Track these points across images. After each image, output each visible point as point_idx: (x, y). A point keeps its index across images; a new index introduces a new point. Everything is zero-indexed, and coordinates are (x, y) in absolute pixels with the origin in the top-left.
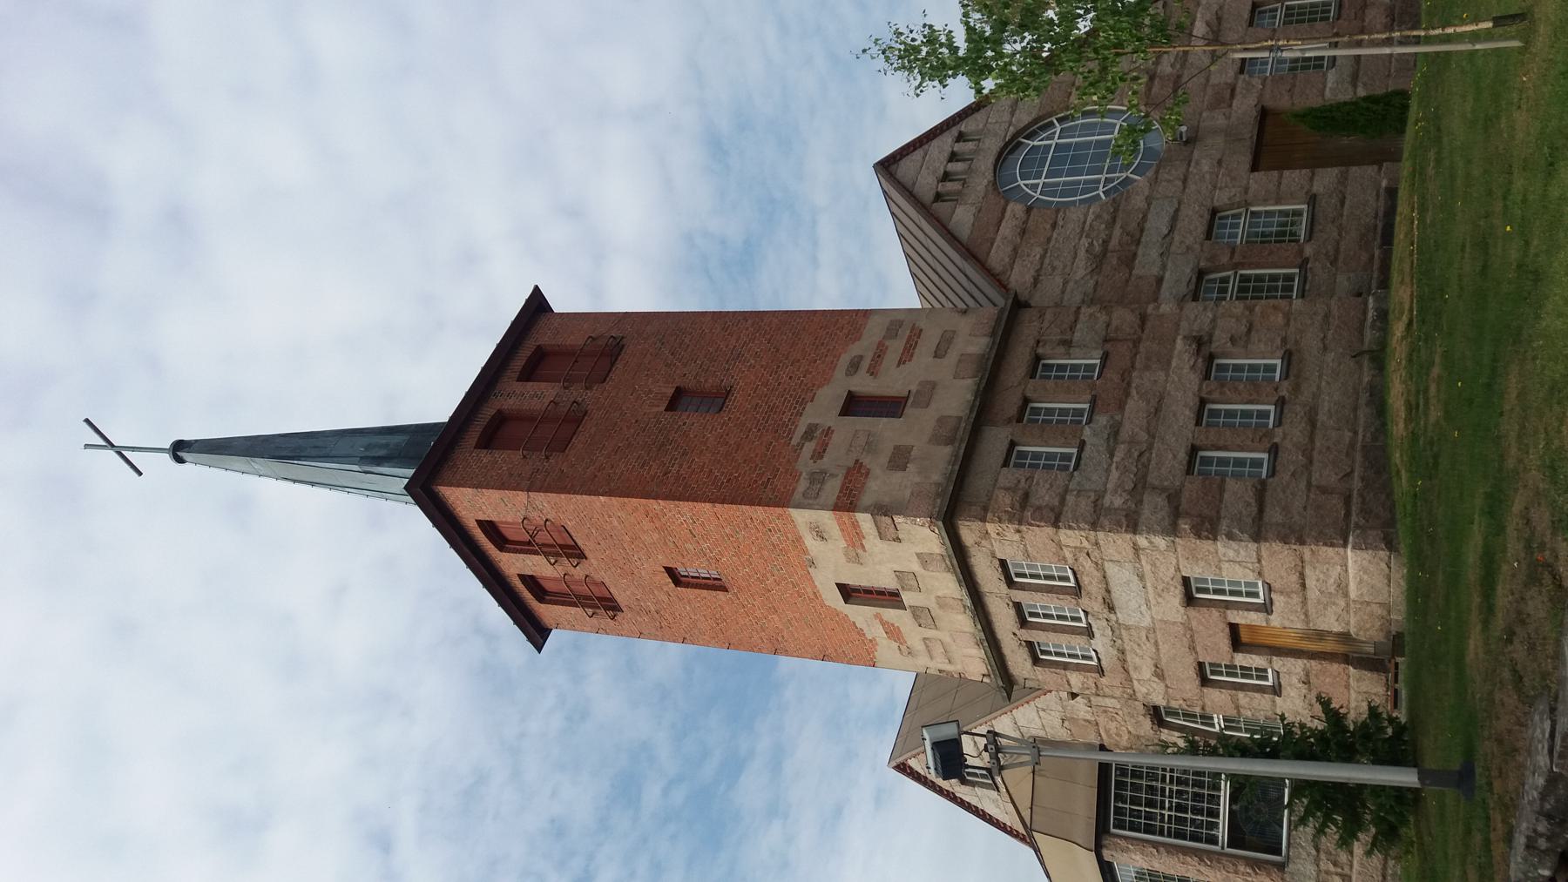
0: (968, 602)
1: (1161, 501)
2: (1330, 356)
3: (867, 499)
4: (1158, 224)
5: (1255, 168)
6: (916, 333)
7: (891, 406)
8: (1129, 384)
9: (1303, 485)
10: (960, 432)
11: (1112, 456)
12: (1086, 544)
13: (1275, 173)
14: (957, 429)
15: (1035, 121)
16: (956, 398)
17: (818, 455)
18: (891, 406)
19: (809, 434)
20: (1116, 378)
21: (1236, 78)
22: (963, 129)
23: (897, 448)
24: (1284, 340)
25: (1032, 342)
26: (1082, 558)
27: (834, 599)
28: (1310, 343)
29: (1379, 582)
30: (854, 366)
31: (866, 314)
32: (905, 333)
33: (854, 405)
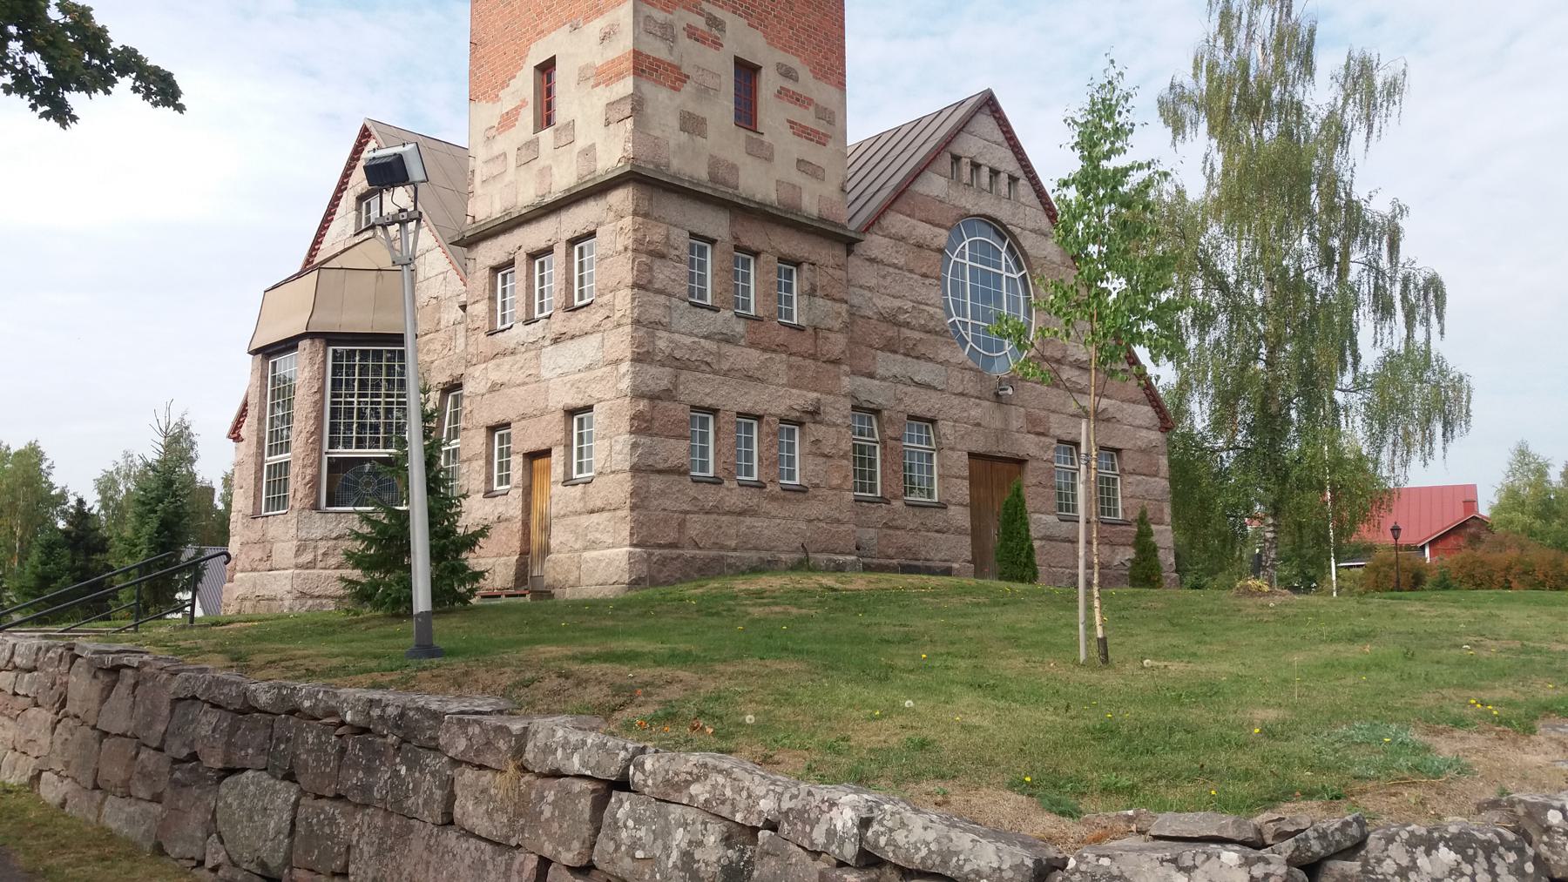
0: (548, 200)
1: (665, 383)
3: (648, 88)
5: (971, 455)
6: (820, 139)
7: (746, 114)
8: (774, 351)
9: (685, 507)
10: (723, 189)
11: (706, 337)
12: (618, 314)
13: (967, 473)
14: (725, 184)
15: (1024, 254)
17: (692, 33)
18: (746, 114)
19: (713, 22)
20: (779, 340)
22: (1021, 181)
23: (704, 120)
24: (817, 486)
25: (813, 258)
26: (604, 312)
27: (538, 55)
28: (815, 509)
29: (599, 576)
30: (788, 73)
31: (842, 85)
33: (746, 72)
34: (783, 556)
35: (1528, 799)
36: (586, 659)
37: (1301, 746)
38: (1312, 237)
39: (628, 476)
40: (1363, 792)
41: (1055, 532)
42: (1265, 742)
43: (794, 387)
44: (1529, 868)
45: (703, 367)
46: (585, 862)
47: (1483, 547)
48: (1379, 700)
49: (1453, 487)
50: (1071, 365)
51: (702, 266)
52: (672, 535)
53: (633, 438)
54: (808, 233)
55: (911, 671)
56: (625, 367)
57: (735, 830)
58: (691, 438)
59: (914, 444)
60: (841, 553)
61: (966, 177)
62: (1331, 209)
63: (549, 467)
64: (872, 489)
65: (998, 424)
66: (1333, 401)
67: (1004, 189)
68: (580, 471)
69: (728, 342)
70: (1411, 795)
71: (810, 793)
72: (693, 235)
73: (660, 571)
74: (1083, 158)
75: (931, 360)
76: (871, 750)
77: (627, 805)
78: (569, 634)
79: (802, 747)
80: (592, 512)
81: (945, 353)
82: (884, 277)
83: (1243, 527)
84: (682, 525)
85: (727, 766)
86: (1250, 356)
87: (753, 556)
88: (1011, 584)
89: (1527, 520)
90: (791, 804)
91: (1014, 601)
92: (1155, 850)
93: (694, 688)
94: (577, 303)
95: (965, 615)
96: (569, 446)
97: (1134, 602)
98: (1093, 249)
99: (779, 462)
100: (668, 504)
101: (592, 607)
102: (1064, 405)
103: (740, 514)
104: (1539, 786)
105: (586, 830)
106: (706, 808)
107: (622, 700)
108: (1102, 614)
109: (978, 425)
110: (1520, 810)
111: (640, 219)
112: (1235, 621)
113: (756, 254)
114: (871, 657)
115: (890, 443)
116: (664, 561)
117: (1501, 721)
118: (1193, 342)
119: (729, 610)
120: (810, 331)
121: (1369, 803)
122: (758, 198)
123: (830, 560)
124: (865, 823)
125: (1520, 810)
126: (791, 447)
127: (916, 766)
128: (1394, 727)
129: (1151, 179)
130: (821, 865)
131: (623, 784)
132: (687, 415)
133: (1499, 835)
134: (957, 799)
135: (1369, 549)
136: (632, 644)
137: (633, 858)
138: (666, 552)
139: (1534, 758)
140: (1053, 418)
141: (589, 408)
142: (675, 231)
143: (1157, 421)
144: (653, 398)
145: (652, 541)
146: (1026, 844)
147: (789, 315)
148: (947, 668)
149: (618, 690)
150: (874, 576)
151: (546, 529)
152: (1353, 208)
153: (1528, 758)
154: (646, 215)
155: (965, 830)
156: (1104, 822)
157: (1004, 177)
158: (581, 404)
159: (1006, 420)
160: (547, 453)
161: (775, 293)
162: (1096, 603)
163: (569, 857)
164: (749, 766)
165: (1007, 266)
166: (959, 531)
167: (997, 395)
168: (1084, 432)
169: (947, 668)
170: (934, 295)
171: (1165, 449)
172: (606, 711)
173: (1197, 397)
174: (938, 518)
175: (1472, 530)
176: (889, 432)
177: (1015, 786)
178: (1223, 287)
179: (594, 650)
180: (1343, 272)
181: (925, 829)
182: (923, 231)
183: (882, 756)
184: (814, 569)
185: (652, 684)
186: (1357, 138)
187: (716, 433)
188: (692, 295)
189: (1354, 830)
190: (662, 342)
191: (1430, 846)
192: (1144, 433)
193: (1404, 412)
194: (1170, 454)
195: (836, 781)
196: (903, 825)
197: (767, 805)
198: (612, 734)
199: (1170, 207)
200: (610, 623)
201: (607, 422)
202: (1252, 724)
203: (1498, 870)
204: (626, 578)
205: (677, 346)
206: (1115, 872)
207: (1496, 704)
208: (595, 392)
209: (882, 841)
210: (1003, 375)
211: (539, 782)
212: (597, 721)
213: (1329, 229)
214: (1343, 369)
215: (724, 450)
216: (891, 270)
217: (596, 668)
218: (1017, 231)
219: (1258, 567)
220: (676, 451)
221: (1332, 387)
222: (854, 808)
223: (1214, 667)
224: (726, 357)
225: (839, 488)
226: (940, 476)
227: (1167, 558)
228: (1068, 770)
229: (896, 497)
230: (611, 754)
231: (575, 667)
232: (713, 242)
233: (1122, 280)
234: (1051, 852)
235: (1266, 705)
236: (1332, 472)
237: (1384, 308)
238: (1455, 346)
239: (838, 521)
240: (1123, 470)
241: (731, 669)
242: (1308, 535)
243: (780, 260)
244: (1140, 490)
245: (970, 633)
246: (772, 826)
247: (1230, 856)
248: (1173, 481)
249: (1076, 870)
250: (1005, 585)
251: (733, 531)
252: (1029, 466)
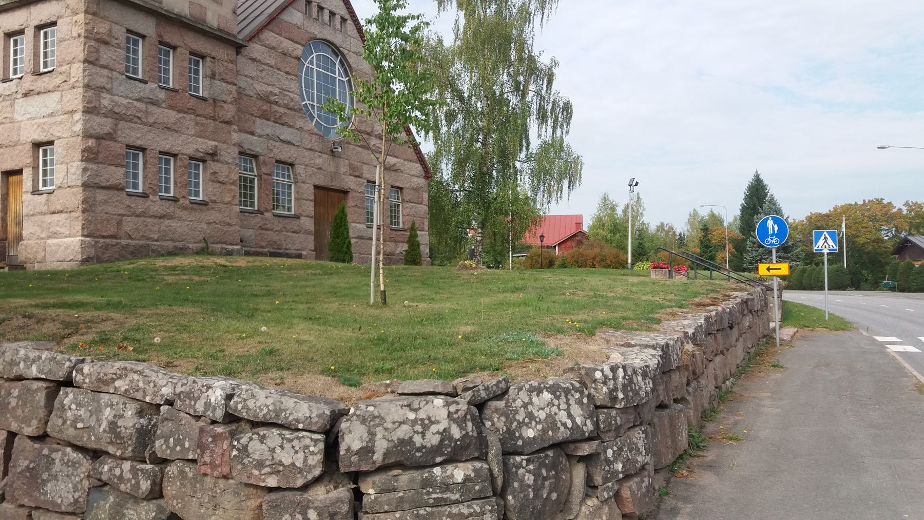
1: (107, 129)
4: (286, 133)
5: (316, 187)
8: (186, 112)
9: (122, 212)
11: (137, 100)
12: (73, 80)
13: (312, 198)
20: (189, 105)
24: (214, 202)
25: (213, 54)
28: (213, 216)
29: (60, 256)
34: (190, 246)
35: (587, 366)
36: (46, 306)
37: (481, 344)
38: (509, 74)
39: (80, 190)
40: (510, 366)
42: (464, 343)
43: (200, 137)
44: (585, 400)
45: (135, 120)
46: (41, 432)
47: (583, 247)
48: (524, 321)
49: (572, 216)
51: (135, 52)
52: (112, 230)
53: (84, 165)
55: (269, 312)
56: (78, 116)
57: (145, 406)
58: (127, 166)
59: (280, 178)
60: (231, 244)
61: (315, 14)
62: (521, 59)
63: (21, 182)
64: (252, 205)
65: (332, 169)
66: (515, 167)
67: (338, 25)
68: (45, 184)
70: (532, 367)
71: (194, 382)
72: (129, 31)
73: (103, 254)
74: (380, 8)
75: (291, 126)
76: (238, 357)
77: (71, 396)
78: (35, 292)
79: (193, 356)
80: (54, 213)
81: (300, 123)
82: (261, 71)
83: (466, 234)
84: (119, 223)
85: (140, 368)
86: (473, 140)
87: (170, 245)
88: (337, 264)
89: (605, 233)
90: (182, 389)
91: (337, 272)
92: (399, 400)
93: (122, 324)
94: (42, 70)
95: (307, 280)
96: (36, 168)
97: (405, 273)
98: (385, 64)
99: (189, 185)
100: (110, 209)
101: (54, 276)
103: (161, 218)
104: (594, 360)
105: (42, 413)
106: (126, 394)
107: (70, 331)
108: (384, 276)
109: (320, 169)
110: (583, 372)
111: (90, 17)
112: (457, 282)
113: (174, 48)
114: (244, 304)
115: (264, 177)
116: (106, 247)
117: (581, 330)
118: (444, 129)
119: (151, 278)
120: (211, 101)
121: (512, 372)
122: (176, 11)
123: (223, 248)
124: (229, 397)
125: (583, 372)
126: (197, 176)
127: (268, 364)
128: (529, 333)
129: (419, 26)
130: (201, 424)
131: (68, 382)
132: (124, 151)
133: (572, 385)
134: (289, 381)
135: (529, 247)
136: (79, 298)
137: (76, 428)
138: (108, 240)
139: (593, 347)
140: (365, 167)
141: (51, 143)
142: (116, 28)
143: (423, 173)
144: (99, 138)
145: (98, 233)
146: (327, 403)
147: (197, 89)
148: (292, 309)
149: (66, 325)
150: (251, 259)
151: (19, 224)
152: (531, 58)
153: (590, 347)
154: (94, 14)
155: (291, 397)
156: (373, 388)
157: (338, 18)
158: (45, 139)
159: (337, 167)
160: (19, 172)
161: (187, 74)
162: (381, 271)
163: (29, 430)
164: (155, 368)
165: (339, 73)
166: (307, 232)
167: (332, 151)
168: (378, 175)
169: (292, 309)
170: (294, 86)
171: (426, 189)
172: (58, 339)
173: (445, 161)
174: (294, 225)
175: (579, 238)
176: (264, 170)
177: (326, 372)
178: (461, 99)
179: (52, 301)
180: (524, 96)
181: (267, 398)
182: (287, 44)
183: (244, 360)
184: (212, 254)
185: (91, 321)
186: (537, 19)
187: (144, 164)
188: (128, 71)
189: (503, 385)
190: (106, 101)
191: (539, 391)
192: (416, 179)
193: (550, 174)
194: (429, 191)
195: (213, 374)
196: (253, 396)
197: (166, 391)
198: (62, 352)
199: (435, 49)
200: (65, 285)
201: (65, 152)
202: (458, 334)
203: (570, 402)
204: (79, 257)
205: (117, 104)
206: (376, 414)
207: (579, 322)
208: (55, 132)
209: (240, 406)
210: (336, 139)
211: (7, 384)
212: (50, 345)
213: (518, 70)
214: (521, 150)
215: (150, 175)
216: (266, 67)
217: (52, 312)
218: (346, 52)
219: (472, 255)
220: (116, 175)
221: (515, 159)
222: (222, 389)
223: (442, 305)
224: (152, 114)
225: (229, 203)
226: (296, 199)
227: (425, 250)
228: (356, 362)
229: (267, 211)
230: (60, 364)
231: (36, 311)
232: (143, 37)
233: (402, 84)
234: (342, 406)
235: (467, 324)
236: (512, 205)
237: (542, 118)
238: (576, 139)
239: (229, 224)
240: (403, 200)
241: (148, 312)
242: (499, 240)
243: (191, 53)
244: (412, 212)
245: (308, 290)
246: (170, 403)
247: (439, 401)
248: (430, 207)
249: (354, 414)
250: (333, 264)
251: (156, 229)
252: (350, 195)
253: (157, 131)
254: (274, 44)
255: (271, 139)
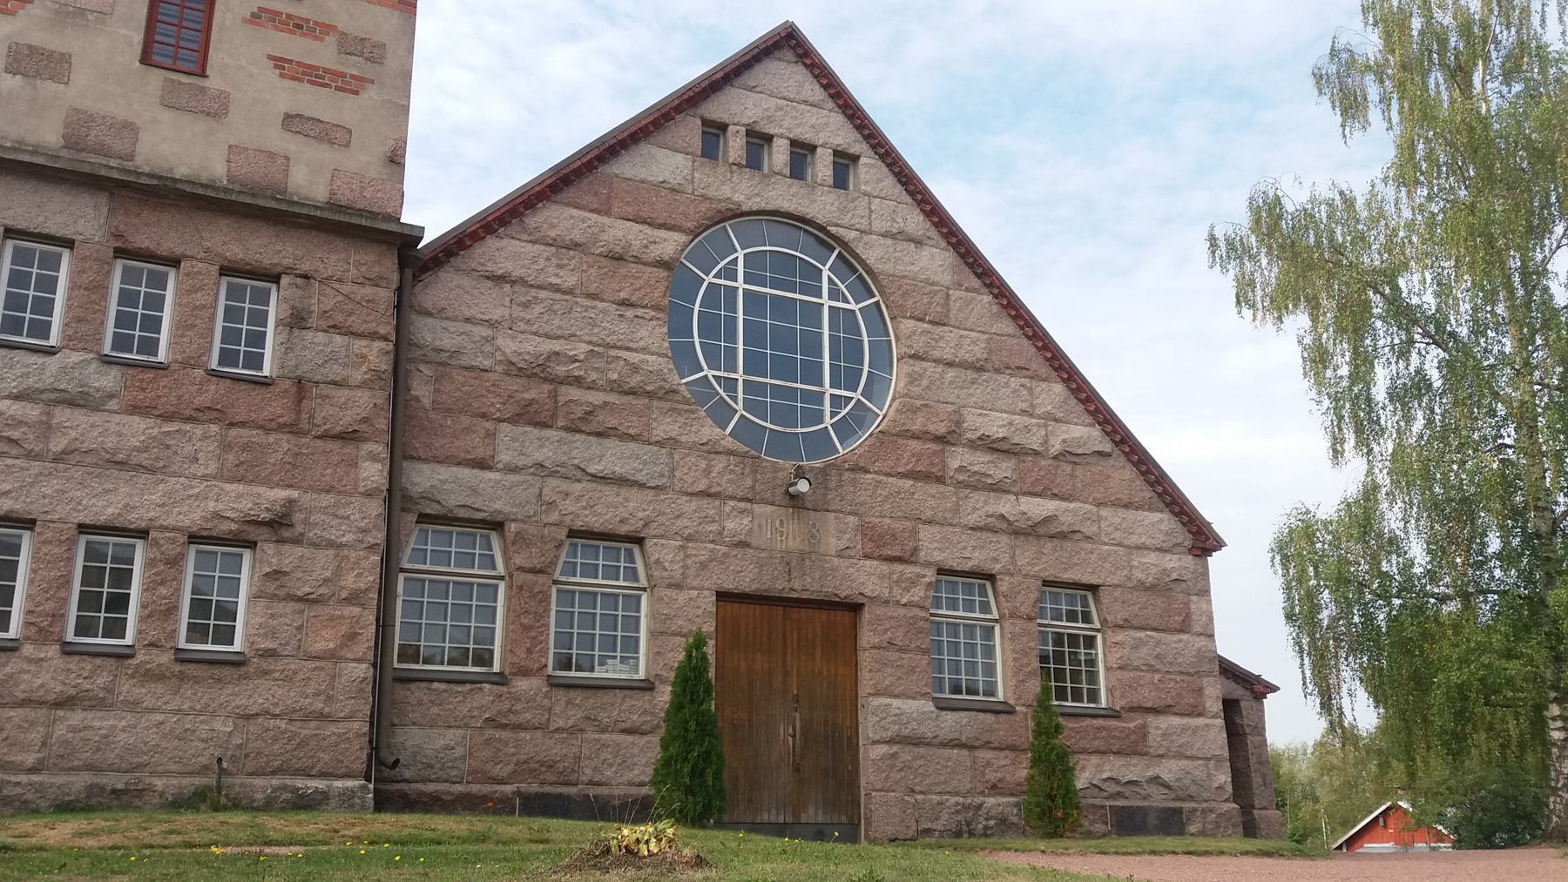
2: (223, 726)
4: (612, 457)
5: (723, 596)
8: (190, 419)
10: (93, 159)
11: (17, 397)
15: (869, 271)
16: (176, 145)
20: (204, 399)
21: (928, 564)
22: (863, 160)
24: (271, 654)
25: (305, 267)
28: (258, 694)
32: (353, 66)
34: (159, 783)
41: (927, 730)
50: (973, 445)
54: (299, 226)
60: (323, 775)
69: (72, 403)
75: (633, 438)
87: (78, 783)
102: (956, 510)
109: (743, 544)
123: (285, 788)
140: (925, 533)
159: (813, 537)
218: (849, 235)
225: (332, 656)
226: (654, 635)
232: (69, 244)
239: (322, 717)
240: (1104, 622)
251: (36, 736)
252: (866, 615)
253: (77, 473)
254: (577, 236)
255: (553, 474)
